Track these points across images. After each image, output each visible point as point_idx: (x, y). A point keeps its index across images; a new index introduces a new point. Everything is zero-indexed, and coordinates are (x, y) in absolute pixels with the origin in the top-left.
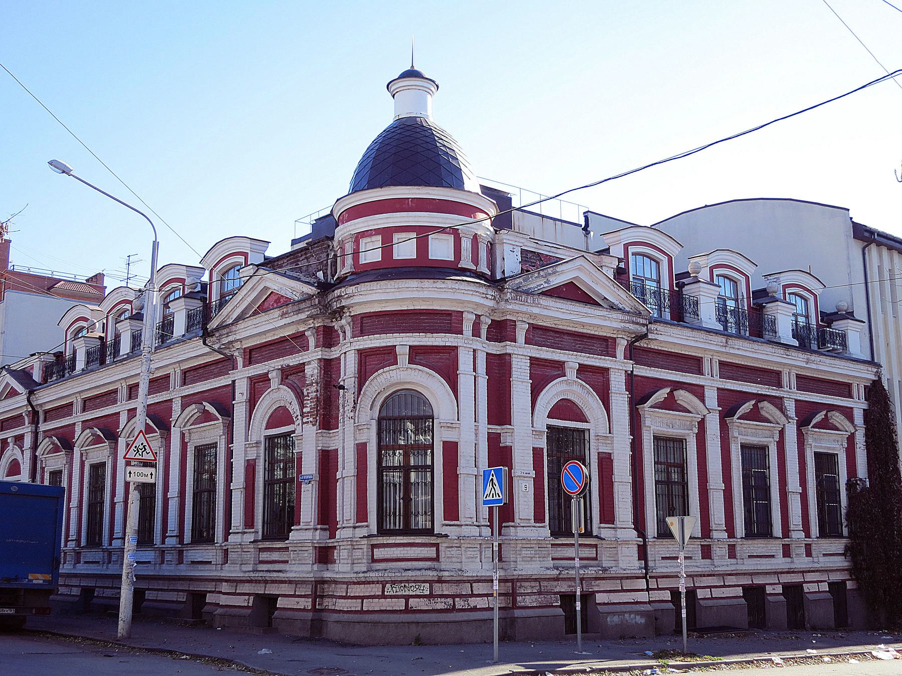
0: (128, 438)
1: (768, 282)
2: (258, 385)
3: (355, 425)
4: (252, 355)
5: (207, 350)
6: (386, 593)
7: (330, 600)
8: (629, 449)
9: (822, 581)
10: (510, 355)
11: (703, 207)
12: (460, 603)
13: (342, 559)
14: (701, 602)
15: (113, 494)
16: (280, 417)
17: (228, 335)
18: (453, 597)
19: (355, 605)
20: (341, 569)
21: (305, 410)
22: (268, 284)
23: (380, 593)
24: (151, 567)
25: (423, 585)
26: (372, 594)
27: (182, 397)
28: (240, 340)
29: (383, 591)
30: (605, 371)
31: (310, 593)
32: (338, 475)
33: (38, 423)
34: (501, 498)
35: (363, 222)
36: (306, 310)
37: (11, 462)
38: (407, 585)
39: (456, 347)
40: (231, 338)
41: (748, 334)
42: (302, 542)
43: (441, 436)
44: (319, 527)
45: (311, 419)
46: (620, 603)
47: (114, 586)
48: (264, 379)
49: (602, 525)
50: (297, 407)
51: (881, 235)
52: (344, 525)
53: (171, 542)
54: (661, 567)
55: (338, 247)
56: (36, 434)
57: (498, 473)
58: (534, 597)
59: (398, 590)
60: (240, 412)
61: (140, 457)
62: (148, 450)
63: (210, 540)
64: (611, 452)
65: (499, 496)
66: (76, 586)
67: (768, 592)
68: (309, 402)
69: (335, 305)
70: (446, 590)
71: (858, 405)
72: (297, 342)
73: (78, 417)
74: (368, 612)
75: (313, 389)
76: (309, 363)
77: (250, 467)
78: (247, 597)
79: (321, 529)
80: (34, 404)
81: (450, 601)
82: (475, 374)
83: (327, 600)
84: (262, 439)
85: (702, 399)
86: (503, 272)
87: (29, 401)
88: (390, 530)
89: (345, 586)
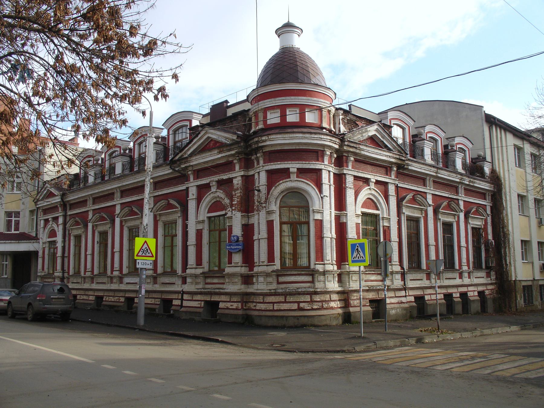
0: (122, 218)
1: (448, 141)
2: (203, 190)
3: (266, 211)
4: (200, 172)
5: (171, 171)
6: (287, 301)
8: (189, 232)
9: (475, 291)
10: (345, 174)
11: (404, 105)
14: (427, 302)
15: (113, 247)
19: (270, 307)
21: (233, 203)
22: (210, 135)
23: (284, 301)
26: (280, 301)
27: (154, 196)
28: (192, 166)
29: (285, 299)
30: (385, 184)
31: (240, 300)
32: (255, 237)
33: (66, 210)
35: (269, 102)
36: (235, 149)
37: (51, 231)
41: (441, 166)
44: (244, 265)
46: (192, 307)
47: (115, 295)
48: (207, 187)
51: (499, 120)
52: (260, 264)
53: (116, 273)
55: (253, 115)
56: (65, 216)
60: (192, 205)
62: (149, 252)
66: (92, 295)
67: (454, 296)
68: (236, 198)
69: (254, 146)
73: (90, 207)
74: (277, 310)
75: (239, 191)
76: (236, 177)
77: (199, 233)
78: (200, 302)
79: (245, 266)
82: (329, 184)
84: (206, 219)
87: (62, 199)
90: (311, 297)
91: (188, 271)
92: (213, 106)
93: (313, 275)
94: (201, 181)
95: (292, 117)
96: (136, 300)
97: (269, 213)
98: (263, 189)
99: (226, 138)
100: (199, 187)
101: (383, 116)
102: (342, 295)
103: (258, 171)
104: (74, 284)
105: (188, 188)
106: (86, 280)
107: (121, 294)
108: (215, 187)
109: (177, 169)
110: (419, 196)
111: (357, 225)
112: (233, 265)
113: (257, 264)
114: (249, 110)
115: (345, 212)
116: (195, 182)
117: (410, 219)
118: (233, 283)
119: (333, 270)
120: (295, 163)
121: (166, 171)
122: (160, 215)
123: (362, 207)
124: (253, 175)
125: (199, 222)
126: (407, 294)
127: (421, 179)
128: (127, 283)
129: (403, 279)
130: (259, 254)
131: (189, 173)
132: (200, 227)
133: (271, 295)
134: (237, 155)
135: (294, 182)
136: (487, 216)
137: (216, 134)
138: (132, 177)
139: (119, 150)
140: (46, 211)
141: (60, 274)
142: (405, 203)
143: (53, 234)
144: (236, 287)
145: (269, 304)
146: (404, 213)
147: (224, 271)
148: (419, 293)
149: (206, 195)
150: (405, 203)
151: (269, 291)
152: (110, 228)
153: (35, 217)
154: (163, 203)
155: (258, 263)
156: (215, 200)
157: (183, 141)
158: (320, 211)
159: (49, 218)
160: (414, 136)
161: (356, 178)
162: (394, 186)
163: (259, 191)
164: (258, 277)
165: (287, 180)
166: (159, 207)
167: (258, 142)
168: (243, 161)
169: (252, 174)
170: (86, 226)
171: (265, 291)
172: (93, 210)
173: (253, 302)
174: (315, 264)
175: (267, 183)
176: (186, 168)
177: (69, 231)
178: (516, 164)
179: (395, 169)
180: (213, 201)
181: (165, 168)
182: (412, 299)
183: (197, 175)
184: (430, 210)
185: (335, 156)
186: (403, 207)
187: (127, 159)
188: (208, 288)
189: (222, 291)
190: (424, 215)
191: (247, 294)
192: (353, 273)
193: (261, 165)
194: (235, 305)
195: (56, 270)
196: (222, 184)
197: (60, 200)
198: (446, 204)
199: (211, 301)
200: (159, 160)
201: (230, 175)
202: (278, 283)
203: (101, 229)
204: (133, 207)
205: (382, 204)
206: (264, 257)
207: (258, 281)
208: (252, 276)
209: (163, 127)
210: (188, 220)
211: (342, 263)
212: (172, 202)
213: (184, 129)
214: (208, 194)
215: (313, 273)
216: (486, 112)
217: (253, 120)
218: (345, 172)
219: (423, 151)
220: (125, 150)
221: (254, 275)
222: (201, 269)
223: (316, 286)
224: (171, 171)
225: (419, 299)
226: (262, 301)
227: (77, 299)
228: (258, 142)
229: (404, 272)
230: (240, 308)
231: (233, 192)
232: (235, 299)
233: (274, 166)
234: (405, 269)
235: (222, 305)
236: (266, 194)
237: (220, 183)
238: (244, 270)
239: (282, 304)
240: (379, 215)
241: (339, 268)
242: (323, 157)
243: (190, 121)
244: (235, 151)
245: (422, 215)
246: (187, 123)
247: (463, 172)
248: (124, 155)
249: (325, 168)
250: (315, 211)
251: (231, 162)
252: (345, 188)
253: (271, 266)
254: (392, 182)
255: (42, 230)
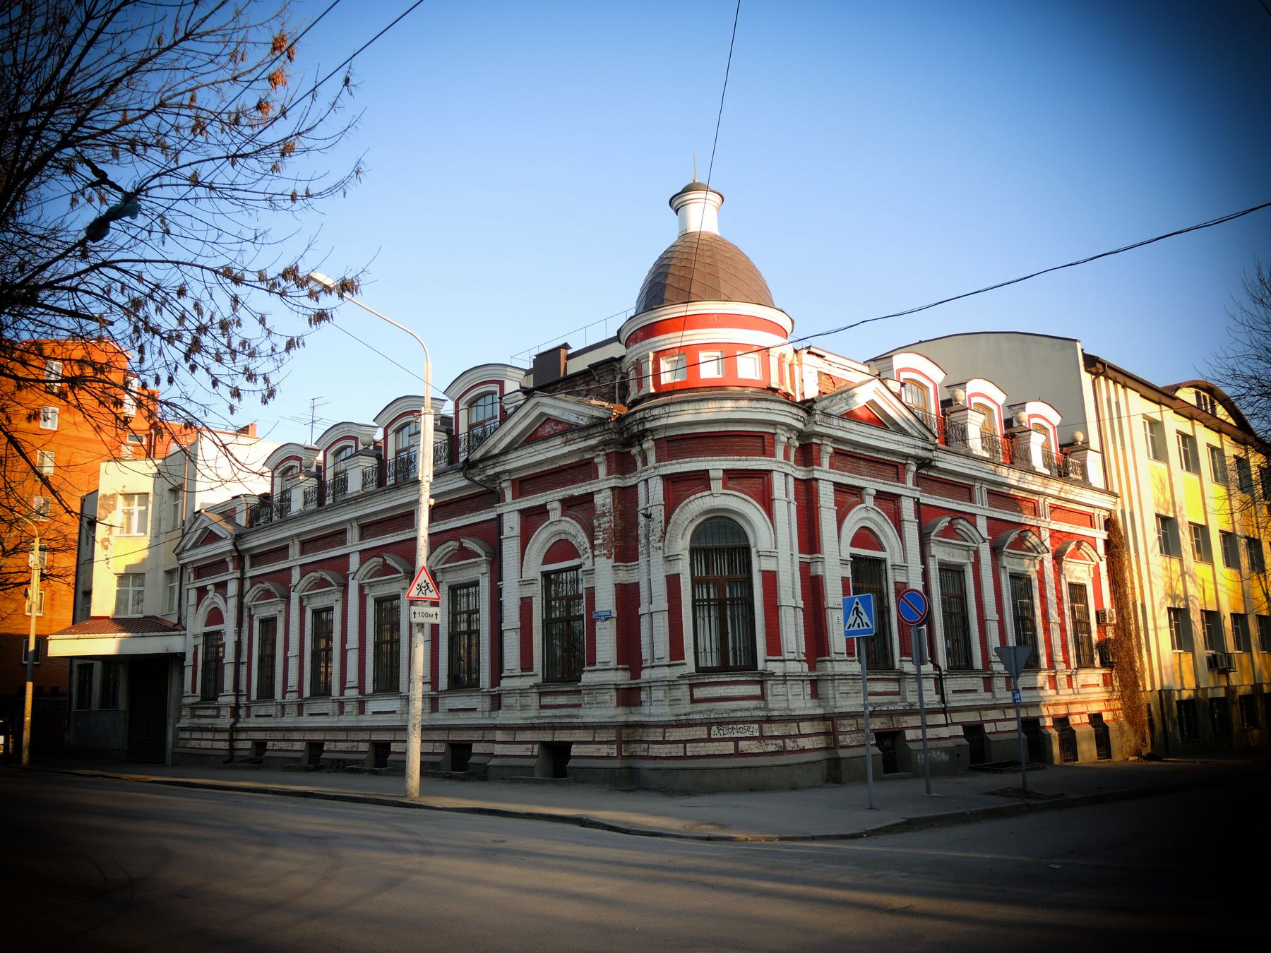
5: (465, 483)
6: (712, 736)
7: (637, 745)
8: (505, 604)
10: (817, 480)
12: (790, 745)
13: (655, 701)
16: (562, 550)
17: (494, 466)
18: (783, 737)
19: (678, 750)
20: (656, 708)
21: (596, 542)
23: (706, 737)
24: (395, 717)
25: (752, 725)
28: (509, 471)
29: (709, 734)
30: (896, 498)
31: (614, 739)
32: (643, 609)
34: (871, 627)
38: (735, 726)
39: (771, 471)
40: (498, 469)
42: (600, 687)
43: (759, 565)
44: (620, 666)
45: (605, 552)
46: (515, 756)
48: (542, 511)
49: (904, 658)
50: (586, 540)
54: (954, 701)
56: (241, 581)
57: (865, 602)
58: (853, 736)
59: (726, 732)
60: (510, 549)
61: (424, 596)
63: (474, 685)
64: (906, 581)
65: (868, 626)
68: (601, 533)
70: (776, 730)
71: (1101, 535)
72: (584, 469)
74: (693, 757)
75: (605, 519)
76: (600, 491)
77: (526, 605)
78: (530, 746)
79: (622, 669)
80: (240, 548)
81: (780, 742)
83: (633, 746)
85: (974, 525)
86: (803, 394)
87: (234, 545)
88: (712, 667)
89: (661, 730)
90: (761, 729)
91: (505, 683)
92: (539, 356)
93: (761, 683)
94: (527, 500)
95: (709, 370)
96: (394, 747)
97: (669, 559)
98: (658, 513)
99: (579, 414)
100: (524, 513)
101: (882, 364)
102: (821, 723)
103: (646, 478)
104: (259, 718)
105: (500, 516)
106: (287, 710)
107: (362, 736)
108: (559, 512)
109: (477, 479)
110: (961, 521)
111: (844, 580)
112: (598, 666)
113: (648, 665)
114: (622, 358)
115: (820, 556)
116: (516, 503)
117: (945, 568)
118: (599, 703)
119: (802, 672)
120: (720, 460)
121: (457, 482)
122: (308, 597)
123: (853, 544)
124: (635, 486)
125: (525, 583)
126: (949, 721)
127: (962, 488)
128: (374, 713)
129: (940, 690)
130: (652, 643)
131: (504, 485)
132: (527, 592)
133: (679, 725)
134: (601, 448)
135: (719, 498)
136: (1098, 560)
137: (563, 408)
138: (384, 498)
139: (354, 445)
140: (202, 570)
141: (232, 700)
142: (935, 536)
143: (215, 616)
144: (606, 710)
145: (675, 746)
146: (934, 556)
147: (580, 681)
148: (972, 717)
149: (539, 529)
150: (935, 536)
151: (674, 718)
152: (337, 601)
153: (177, 584)
154: (375, 561)
155: (649, 661)
156: (557, 538)
157: (487, 423)
158: (772, 554)
159: (206, 586)
160: (946, 403)
161: (838, 487)
162: (912, 502)
163: (648, 516)
164: (650, 691)
165: (704, 493)
166: (441, 556)
167: (643, 420)
168: (614, 459)
169: (634, 483)
170: (287, 599)
171: (666, 719)
172: (301, 566)
173: (641, 742)
174: (766, 661)
175: (664, 500)
176: (498, 475)
177: (250, 609)
178: (1149, 455)
179: (914, 468)
180: (553, 541)
181: (453, 477)
182: (959, 731)
183: (520, 489)
184: (985, 551)
185: (797, 444)
186: (932, 545)
187: (371, 462)
188: (547, 717)
189: (575, 720)
190: (972, 560)
191: (628, 725)
192: (841, 677)
193: (650, 465)
194: (604, 750)
195: (223, 692)
196: (579, 506)
197: (231, 547)
198: (1017, 536)
199: (553, 742)
200: (439, 462)
201: (588, 487)
202: (693, 701)
203: (319, 603)
204: (386, 558)
205: (891, 538)
206: (662, 648)
207: (651, 698)
208: (639, 689)
209: (444, 397)
210: (501, 580)
211: (818, 659)
212: (469, 544)
213: (489, 399)
214: (543, 526)
215: (763, 679)
216: (1086, 352)
217: (632, 375)
218: (816, 475)
219: (964, 431)
220: (367, 445)
221: (642, 685)
222: (530, 678)
223: (770, 706)
224: (465, 483)
225: (974, 730)
226: (661, 739)
227: (267, 750)
228: (643, 420)
229: (941, 674)
230: (615, 755)
231: (595, 521)
232: (602, 736)
233: (677, 466)
234: (943, 670)
235: (577, 750)
236: (663, 522)
237: (569, 505)
238: (621, 677)
239: (702, 744)
240: (884, 560)
241: (812, 667)
242: (773, 445)
243: (501, 383)
244: (599, 438)
245: (969, 559)
246: (496, 388)
247: (1047, 472)
248: (365, 453)
249: (778, 469)
250: (761, 553)
251: (590, 461)
252: (818, 508)
253: (678, 667)
254: (908, 494)
255: (191, 610)
